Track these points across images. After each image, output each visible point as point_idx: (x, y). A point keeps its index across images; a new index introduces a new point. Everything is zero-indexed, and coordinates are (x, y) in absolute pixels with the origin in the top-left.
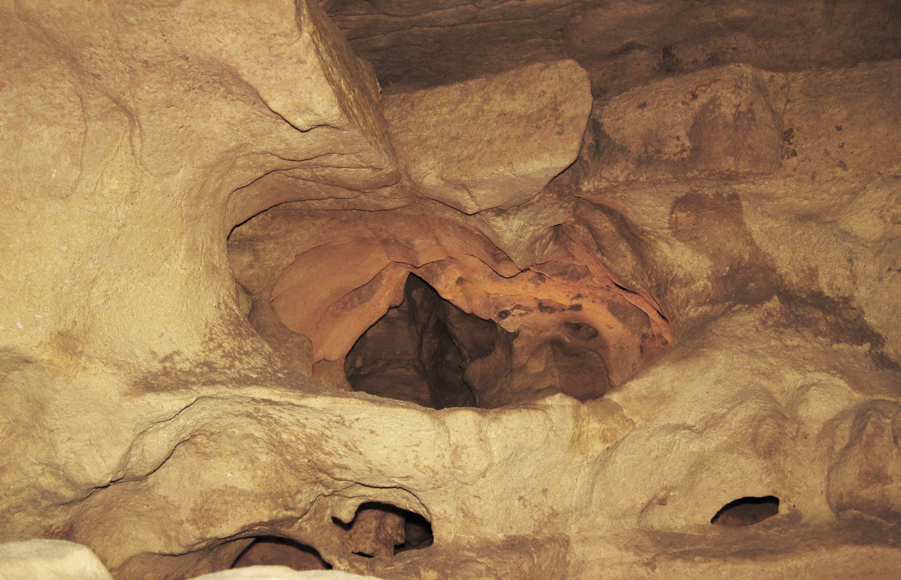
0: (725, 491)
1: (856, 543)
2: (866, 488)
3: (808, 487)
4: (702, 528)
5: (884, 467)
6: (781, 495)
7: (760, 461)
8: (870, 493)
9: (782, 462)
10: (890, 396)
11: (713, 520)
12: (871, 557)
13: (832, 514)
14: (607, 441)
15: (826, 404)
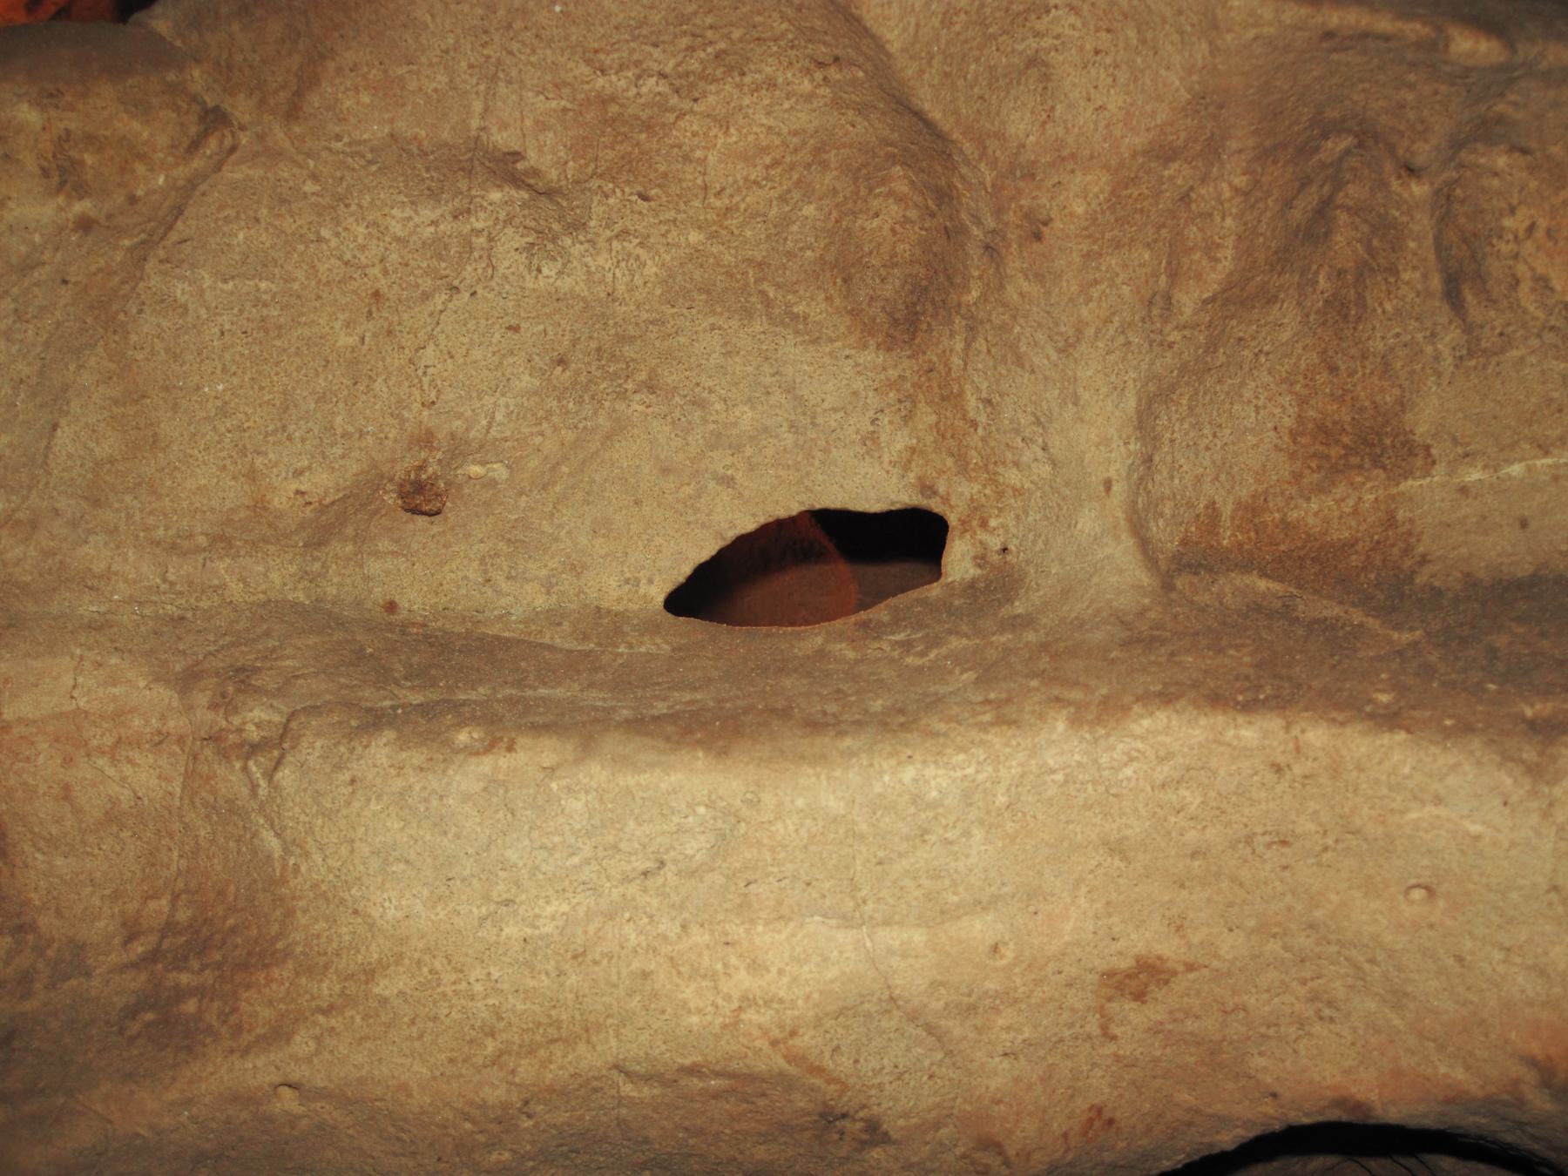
0: (728, 481)
1: (1216, 701)
2: (1320, 489)
3: (1054, 463)
4: (607, 624)
5: (1402, 404)
6: (954, 498)
7: (869, 357)
8: (1335, 510)
9: (956, 361)
10: (1400, 16)
11: (682, 601)
12: (1278, 769)
13: (1146, 579)
14: (81, 190)
15: (1123, 75)
